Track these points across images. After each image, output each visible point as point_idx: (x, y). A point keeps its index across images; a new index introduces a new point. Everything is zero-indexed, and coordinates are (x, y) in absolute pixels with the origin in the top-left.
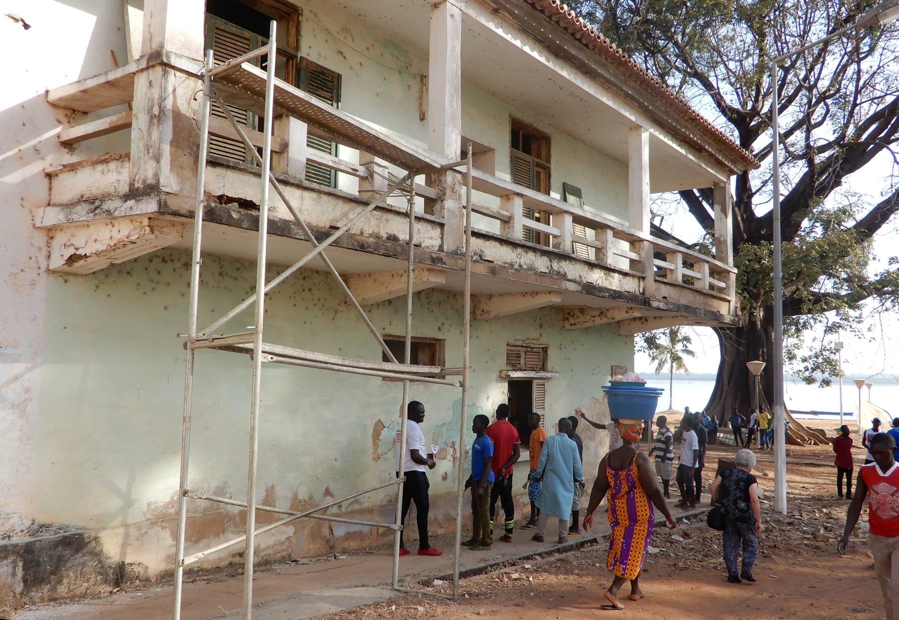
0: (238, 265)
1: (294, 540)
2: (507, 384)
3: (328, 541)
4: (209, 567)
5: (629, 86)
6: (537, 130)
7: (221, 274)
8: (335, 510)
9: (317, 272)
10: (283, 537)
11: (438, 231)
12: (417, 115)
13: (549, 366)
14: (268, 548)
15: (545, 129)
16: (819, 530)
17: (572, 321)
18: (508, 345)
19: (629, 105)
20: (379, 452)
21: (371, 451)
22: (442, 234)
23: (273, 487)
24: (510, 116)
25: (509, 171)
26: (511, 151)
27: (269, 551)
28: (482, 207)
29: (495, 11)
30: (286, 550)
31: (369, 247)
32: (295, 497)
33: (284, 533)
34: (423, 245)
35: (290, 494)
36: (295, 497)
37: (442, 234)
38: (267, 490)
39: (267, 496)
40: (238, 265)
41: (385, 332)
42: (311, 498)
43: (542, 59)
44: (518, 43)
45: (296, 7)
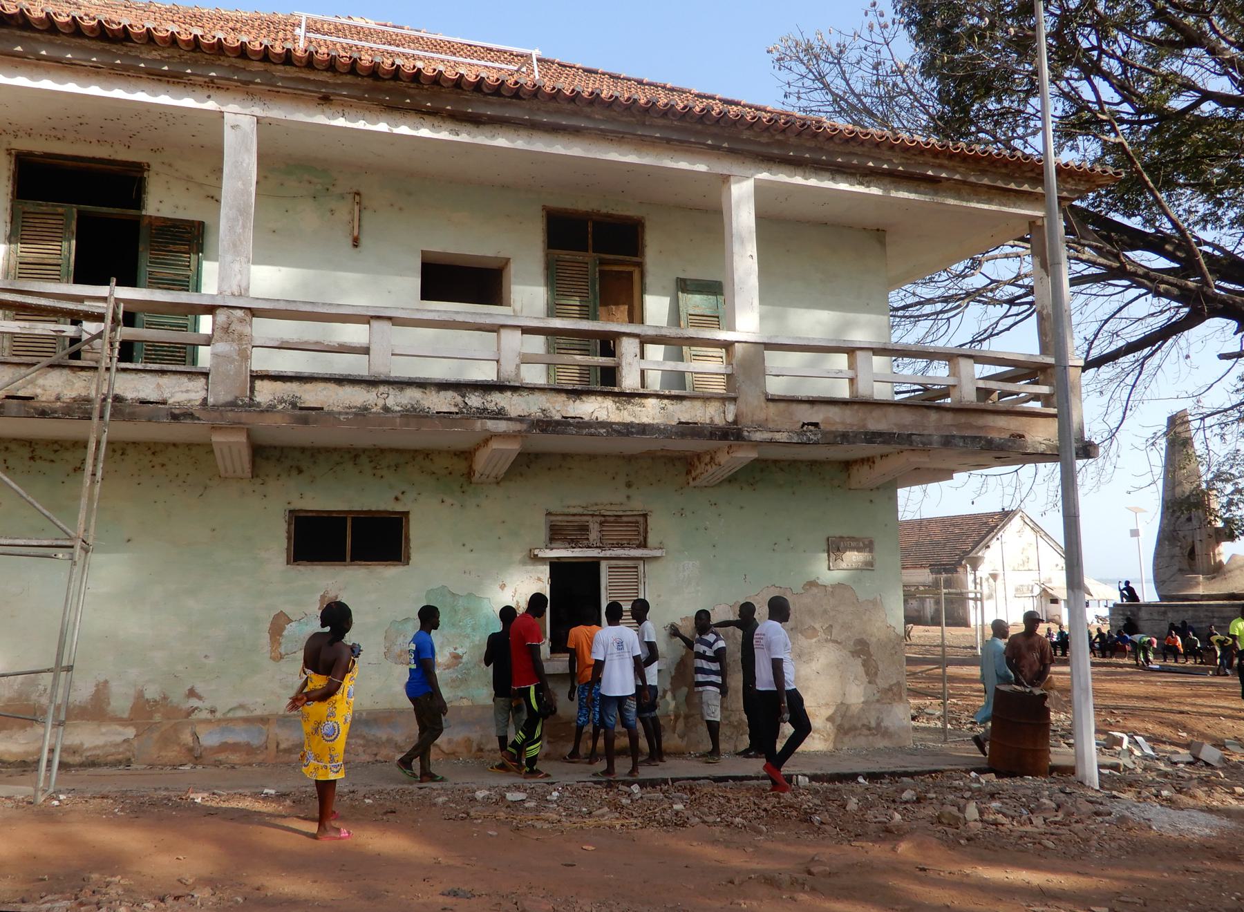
0: (56, 447)
1: (135, 743)
2: (548, 568)
3: (191, 750)
4: (12, 760)
5: (651, 126)
6: (611, 216)
7: (32, 458)
8: (205, 715)
9: (174, 445)
10: (119, 739)
11: (203, 380)
12: (350, 242)
13: (652, 540)
14: (95, 748)
15: (632, 212)
16: (690, 804)
17: (694, 474)
18: (549, 514)
19: (687, 151)
20: (282, 650)
21: (267, 648)
22: (207, 384)
23: (106, 682)
24: (544, 208)
25: (542, 280)
26: (547, 255)
27: (98, 752)
28: (306, 342)
29: (325, 100)
30: (122, 753)
31: (56, 412)
32: (140, 695)
33: (119, 734)
34: (170, 401)
35: (132, 692)
36: (140, 695)
37: (207, 384)
38: (97, 685)
39: (97, 691)
40: (56, 447)
41: (291, 507)
42: (165, 698)
43: (444, 135)
44: (382, 127)
45: (140, 163)
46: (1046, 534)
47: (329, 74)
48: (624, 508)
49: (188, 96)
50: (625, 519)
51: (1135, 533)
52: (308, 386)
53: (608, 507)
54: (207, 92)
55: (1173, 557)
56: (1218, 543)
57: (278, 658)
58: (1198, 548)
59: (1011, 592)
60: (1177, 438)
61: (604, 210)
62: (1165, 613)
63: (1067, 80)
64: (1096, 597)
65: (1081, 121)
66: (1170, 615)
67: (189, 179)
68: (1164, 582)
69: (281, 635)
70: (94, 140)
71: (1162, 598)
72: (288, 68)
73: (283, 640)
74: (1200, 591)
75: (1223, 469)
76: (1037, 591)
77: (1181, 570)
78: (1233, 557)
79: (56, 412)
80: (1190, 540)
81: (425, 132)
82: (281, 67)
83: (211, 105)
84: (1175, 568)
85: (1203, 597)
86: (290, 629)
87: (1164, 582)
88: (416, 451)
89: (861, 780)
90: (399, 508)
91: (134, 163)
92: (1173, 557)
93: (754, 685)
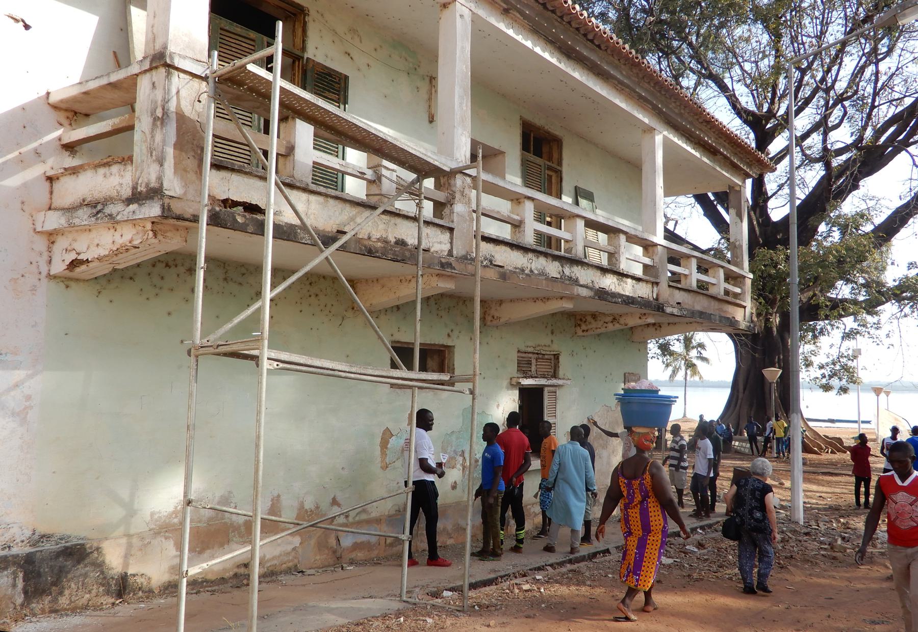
0: (243, 270)
1: (300, 550)
2: (517, 392)
3: (335, 552)
4: (213, 578)
5: (642, 87)
6: (548, 133)
7: (225, 279)
8: (342, 520)
9: (324, 277)
10: (289, 548)
11: (447, 235)
12: (426, 117)
13: (561, 373)
14: (273, 558)
15: (557, 131)
17: (584, 327)
18: (519, 351)
19: (642, 107)
20: (387, 460)
21: (379, 459)
22: (452, 238)
23: (279, 496)
24: (521, 118)
25: (519, 174)
26: (522, 154)
27: (275, 562)
28: (493, 211)
29: (506, 12)
30: (292, 561)
31: (377, 252)
32: (302, 506)
33: (290, 543)
34: (432, 250)
35: (296, 504)
36: (302, 506)
37: (452, 238)
38: (272, 500)
39: (272, 505)
40: (243, 270)
41: (394, 339)
42: (317, 507)
43: (554, 61)
44: (529, 44)
45: (303, 7)
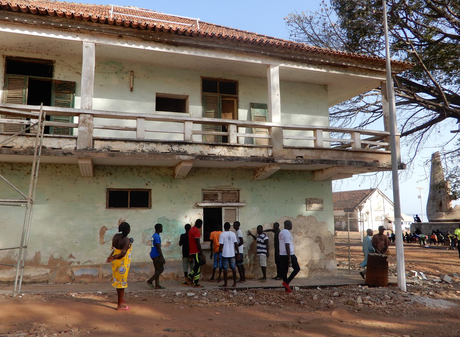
0: (21, 165)
1: (50, 275)
2: (202, 210)
3: (71, 277)
4: (4, 281)
5: (241, 47)
6: (226, 80)
7: (12, 169)
8: (76, 264)
9: (65, 164)
10: (44, 273)
11: (75, 141)
12: (129, 89)
13: (241, 199)
14: (35, 276)
15: (234, 78)
16: (255, 297)
17: (256, 175)
18: (203, 190)
19: (254, 56)
20: (104, 240)
21: (99, 240)
22: (77, 142)
23: (39, 252)
24: (201, 77)
25: (200, 103)
26: (202, 94)
27: (36, 278)
28: (113, 127)
29: (120, 37)
30: (45, 278)
31: (21, 152)
32: (52, 257)
33: (44, 271)
34: (63, 148)
35: (49, 256)
36: (52, 257)
37: (77, 142)
38: (36, 253)
39: (36, 255)
40: (21, 165)
41: (108, 187)
42: (61, 258)
43: (164, 50)
44: (141, 47)
45: (52, 60)
46: (387, 197)
47: (122, 27)
48: (231, 188)
49: (70, 36)
50: (231, 192)
51: (420, 197)
52: (114, 143)
53: (225, 187)
54: (76, 34)
55: (434, 206)
56: (450, 201)
57: (103, 243)
58: (443, 203)
59: (374, 219)
60: (435, 162)
61: (223, 78)
62: (431, 226)
63: (395, 29)
64: (405, 220)
65: (400, 45)
66: (433, 227)
67: (70, 66)
68: (430, 215)
69: (104, 235)
70: (35, 52)
71: (430, 221)
72: (107, 25)
73: (104, 237)
74: (444, 218)
75: (452, 173)
76: (383, 218)
77: (437, 211)
78: (456, 206)
79: (21, 152)
80: (440, 200)
81: (157, 49)
82: (104, 25)
83: (78, 39)
84: (435, 210)
85: (445, 221)
86: (107, 232)
87: (430, 215)
88: (154, 167)
89: (318, 288)
90: (147, 188)
91: (50, 60)
92: (434, 206)
93: (279, 253)
